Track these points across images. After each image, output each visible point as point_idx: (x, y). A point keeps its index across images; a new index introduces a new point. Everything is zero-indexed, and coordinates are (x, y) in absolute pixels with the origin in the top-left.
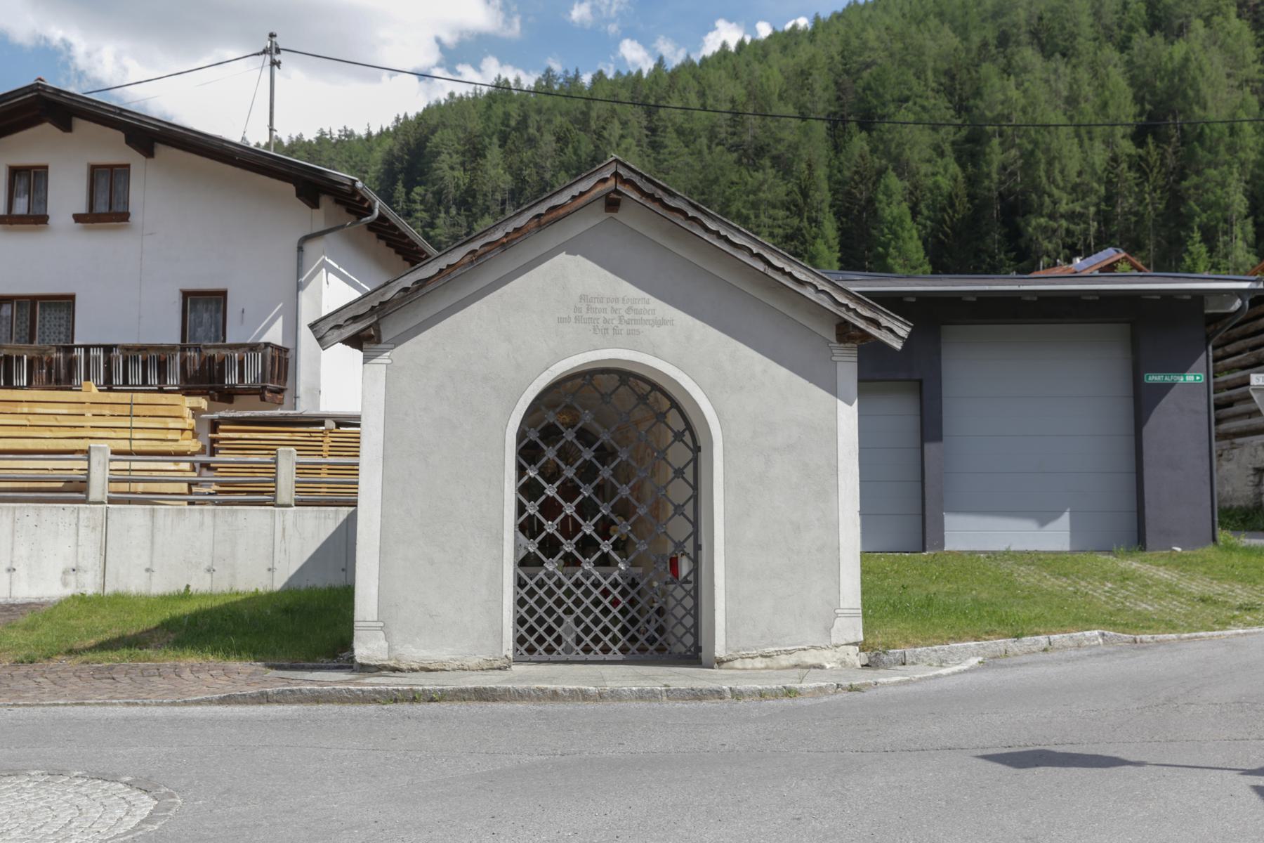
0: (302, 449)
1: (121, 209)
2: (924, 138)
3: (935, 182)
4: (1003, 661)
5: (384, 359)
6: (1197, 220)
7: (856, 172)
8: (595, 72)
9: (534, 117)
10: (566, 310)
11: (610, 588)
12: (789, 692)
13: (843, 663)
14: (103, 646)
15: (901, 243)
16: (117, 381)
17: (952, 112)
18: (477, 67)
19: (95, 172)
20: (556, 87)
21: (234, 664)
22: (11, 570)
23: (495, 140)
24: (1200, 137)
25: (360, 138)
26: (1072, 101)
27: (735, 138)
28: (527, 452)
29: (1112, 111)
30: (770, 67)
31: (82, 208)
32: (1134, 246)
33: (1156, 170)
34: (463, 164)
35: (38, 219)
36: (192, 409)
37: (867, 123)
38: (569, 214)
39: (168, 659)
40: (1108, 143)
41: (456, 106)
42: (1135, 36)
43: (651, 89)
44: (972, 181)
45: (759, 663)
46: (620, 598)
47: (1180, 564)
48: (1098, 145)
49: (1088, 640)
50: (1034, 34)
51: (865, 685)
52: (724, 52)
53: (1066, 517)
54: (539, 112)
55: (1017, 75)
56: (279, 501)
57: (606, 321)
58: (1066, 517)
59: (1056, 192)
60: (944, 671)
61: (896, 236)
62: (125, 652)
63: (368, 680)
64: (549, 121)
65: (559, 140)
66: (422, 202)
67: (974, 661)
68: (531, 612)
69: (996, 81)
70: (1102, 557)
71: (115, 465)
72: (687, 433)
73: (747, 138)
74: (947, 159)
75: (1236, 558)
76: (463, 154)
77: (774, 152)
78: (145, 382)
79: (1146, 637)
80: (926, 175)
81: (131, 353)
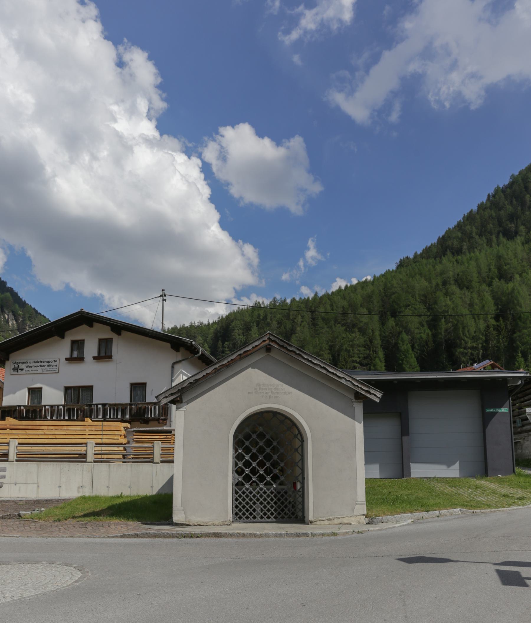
0: (163, 442)
1: (109, 354)
2: (416, 320)
3: (421, 336)
4: (421, 521)
5: (183, 409)
6: (520, 348)
7: (391, 333)
8: (292, 298)
9: (269, 315)
10: (253, 388)
11: (270, 494)
12: (334, 534)
13: (359, 522)
14: (85, 515)
15: (408, 359)
16: (107, 417)
17: (426, 310)
18: (248, 297)
19: (100, 341)
20: (277, 304)
21: (131, 523)
22: (60, 487)
23: (255, 324)
24: (520, 318)
25: (205, 325)
26: (471, 305)
27: (344, 321)
28: (238, 442)
29: (486, 308)
30: (357, 295)
31: (96, 354)
32: (496, 359)
33: (504, 330)
34: (243, 333)
35: (80, 359)
36: (124, 427)
37: (394, 314)
38: (251, 354)
39: (106, 520)
40: (485, 320)
41: (240, 313)
42: (494, 281)
43: (312, 304)
44: (435, 336)
45: (326, 522)
46: (274, 498)
47: (501, 482)
48: (482, 321)
49: (455, 512)
50: (456, 281)
51: (364, 531)
52: (340, 290)
53: (457, 464)
54: (271, 313)
55: (450, 296)
56: (155, 461)
57: (266, 393)
58: (457, 464)
59: (466, 339)
60: (397, 525)
61: (406, 357)
62: (92, 518)
63: (176, 529)
64: (275, 317)
65: (278, 323)
66: (228, 348)
67: (410, 521)
68: (240, 503)
69: (442, 298)
70: (471, 479)
71: (96, 448)
72: (299, 435)
73: (349, 321)
74: (425, 328)
75: (522, 479)
76: (243, 330)
77: (359, 326)
78: (117, 417)
79: (478, 511)
80: (417, 334)
81: (112, 406)
